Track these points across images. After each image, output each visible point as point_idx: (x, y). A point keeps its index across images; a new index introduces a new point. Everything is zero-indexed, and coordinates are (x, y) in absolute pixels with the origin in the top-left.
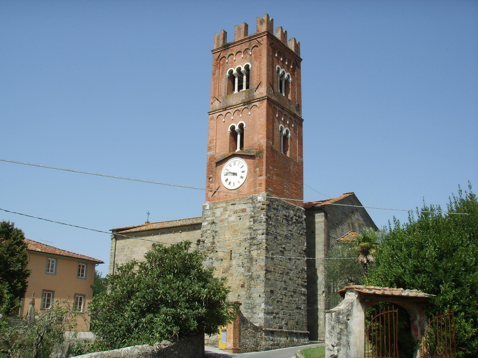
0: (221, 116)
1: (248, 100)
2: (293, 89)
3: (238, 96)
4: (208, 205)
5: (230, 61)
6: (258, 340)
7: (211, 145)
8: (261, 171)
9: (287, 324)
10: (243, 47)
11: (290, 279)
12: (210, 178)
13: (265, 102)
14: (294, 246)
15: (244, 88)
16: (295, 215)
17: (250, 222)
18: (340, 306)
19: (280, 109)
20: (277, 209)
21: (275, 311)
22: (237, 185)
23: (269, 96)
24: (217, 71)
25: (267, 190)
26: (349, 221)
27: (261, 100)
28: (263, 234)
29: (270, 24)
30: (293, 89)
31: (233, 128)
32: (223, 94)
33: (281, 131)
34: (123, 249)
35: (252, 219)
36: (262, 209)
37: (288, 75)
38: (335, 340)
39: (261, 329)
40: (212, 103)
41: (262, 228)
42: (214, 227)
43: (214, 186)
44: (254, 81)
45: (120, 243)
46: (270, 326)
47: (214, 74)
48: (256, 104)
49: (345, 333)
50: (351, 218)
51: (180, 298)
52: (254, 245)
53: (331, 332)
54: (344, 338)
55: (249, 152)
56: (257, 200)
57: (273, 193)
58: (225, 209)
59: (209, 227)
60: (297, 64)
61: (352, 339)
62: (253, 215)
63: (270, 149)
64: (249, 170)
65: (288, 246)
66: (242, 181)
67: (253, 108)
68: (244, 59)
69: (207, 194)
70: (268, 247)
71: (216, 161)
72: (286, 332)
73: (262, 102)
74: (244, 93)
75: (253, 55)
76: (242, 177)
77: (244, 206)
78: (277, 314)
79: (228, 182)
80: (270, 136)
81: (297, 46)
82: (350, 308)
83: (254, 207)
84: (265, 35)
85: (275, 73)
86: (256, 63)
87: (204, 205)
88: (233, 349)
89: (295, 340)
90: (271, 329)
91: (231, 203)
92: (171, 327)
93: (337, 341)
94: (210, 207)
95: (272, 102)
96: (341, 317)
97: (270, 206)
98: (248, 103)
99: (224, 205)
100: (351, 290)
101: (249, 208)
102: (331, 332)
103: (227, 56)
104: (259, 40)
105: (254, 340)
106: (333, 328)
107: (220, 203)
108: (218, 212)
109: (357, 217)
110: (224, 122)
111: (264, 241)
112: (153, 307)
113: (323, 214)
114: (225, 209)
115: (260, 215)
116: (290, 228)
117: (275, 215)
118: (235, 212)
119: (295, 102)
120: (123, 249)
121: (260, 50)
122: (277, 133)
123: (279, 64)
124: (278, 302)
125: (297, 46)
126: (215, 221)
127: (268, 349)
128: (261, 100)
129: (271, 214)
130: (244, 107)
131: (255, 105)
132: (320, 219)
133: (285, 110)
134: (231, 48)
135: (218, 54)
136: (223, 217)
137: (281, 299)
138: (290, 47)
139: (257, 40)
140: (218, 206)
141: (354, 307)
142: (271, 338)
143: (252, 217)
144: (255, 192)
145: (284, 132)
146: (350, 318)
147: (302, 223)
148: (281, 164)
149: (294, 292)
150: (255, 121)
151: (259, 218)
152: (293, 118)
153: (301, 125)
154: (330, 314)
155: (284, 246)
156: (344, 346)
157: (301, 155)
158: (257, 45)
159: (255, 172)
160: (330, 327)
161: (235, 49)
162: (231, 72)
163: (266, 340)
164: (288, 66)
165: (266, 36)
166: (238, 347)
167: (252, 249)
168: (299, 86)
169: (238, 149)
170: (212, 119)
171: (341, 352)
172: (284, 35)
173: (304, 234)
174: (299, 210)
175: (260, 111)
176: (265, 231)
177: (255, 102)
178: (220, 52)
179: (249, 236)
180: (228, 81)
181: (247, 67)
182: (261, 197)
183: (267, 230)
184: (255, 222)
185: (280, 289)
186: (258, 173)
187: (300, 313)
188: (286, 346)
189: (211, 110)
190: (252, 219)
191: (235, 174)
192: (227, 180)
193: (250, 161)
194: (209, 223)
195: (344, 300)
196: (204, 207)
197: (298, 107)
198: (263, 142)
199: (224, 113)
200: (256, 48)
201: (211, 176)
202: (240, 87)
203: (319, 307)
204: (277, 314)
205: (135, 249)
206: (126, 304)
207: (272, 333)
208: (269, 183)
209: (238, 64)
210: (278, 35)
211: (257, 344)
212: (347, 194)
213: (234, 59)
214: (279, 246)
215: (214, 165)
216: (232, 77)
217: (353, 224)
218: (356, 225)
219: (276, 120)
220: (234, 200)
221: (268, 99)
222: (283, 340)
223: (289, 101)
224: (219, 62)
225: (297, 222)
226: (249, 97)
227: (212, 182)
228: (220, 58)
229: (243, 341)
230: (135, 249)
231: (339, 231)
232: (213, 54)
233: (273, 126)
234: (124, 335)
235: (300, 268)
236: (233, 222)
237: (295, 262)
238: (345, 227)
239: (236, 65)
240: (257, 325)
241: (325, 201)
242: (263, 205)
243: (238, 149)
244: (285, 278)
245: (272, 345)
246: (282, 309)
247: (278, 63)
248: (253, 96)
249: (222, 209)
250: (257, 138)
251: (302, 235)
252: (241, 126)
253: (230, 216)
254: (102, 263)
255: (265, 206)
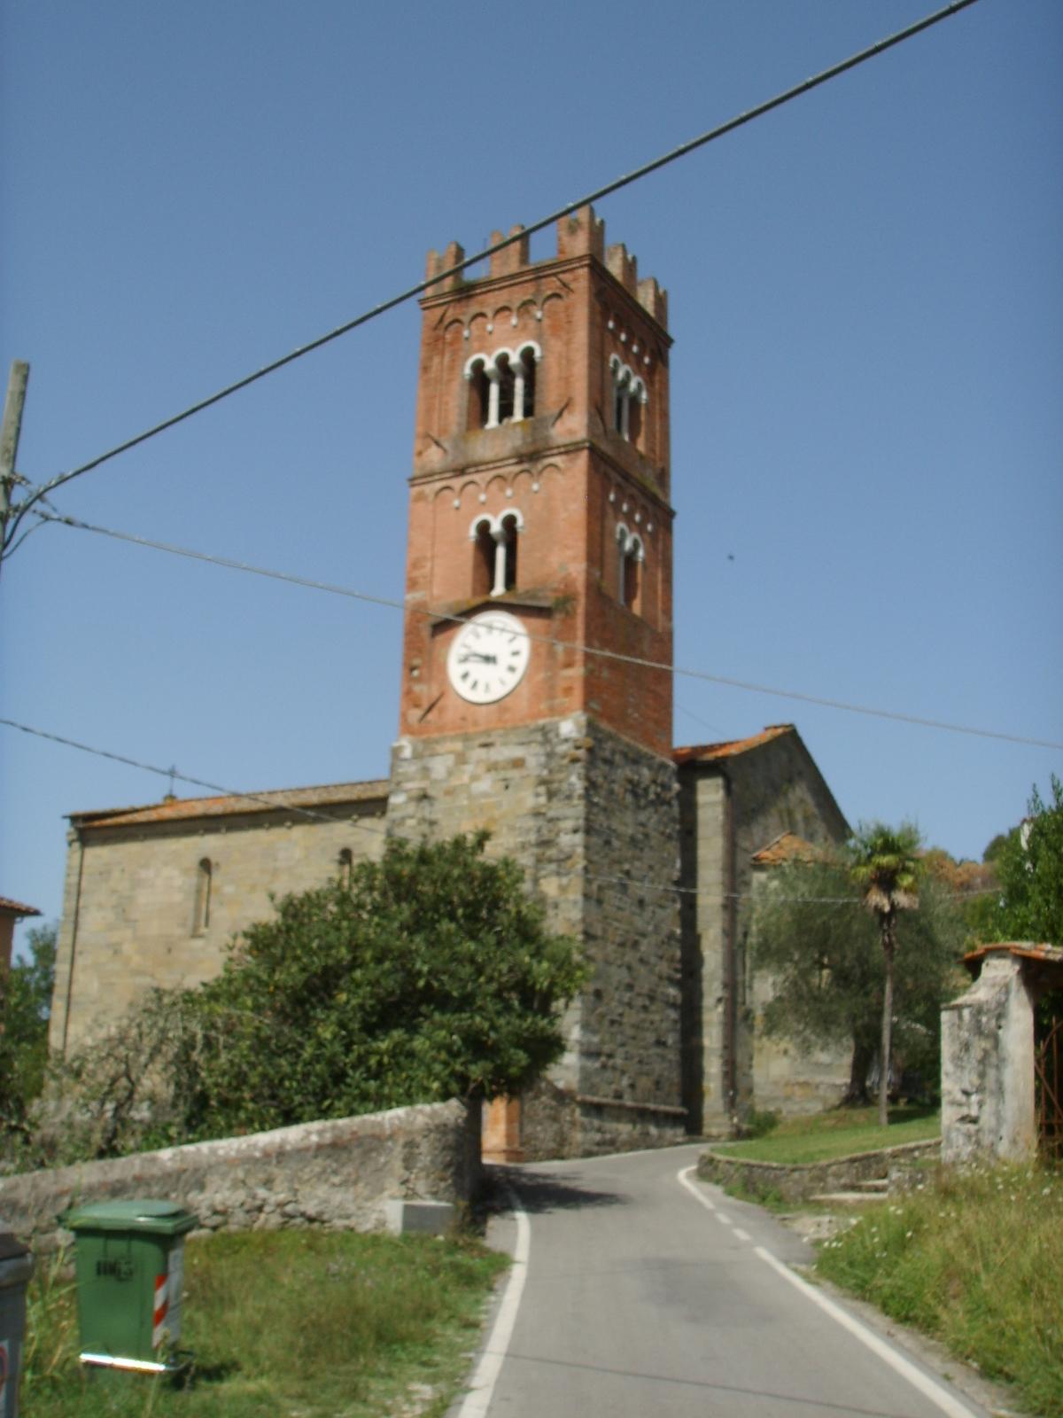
0: (446, 492)
1: (531, 449)
2: (650, 424)
3: (499, 436)
4: (407, 746)
5: (476, 333)
6: (566, 1129)
7: (416, 573)
8: (570, 652)
9: (632, 1086)
10: (517, 296)
11: (642, 961)
12: (412, 669)
13: (583, 457)
14: (651, 868)
15: (518, 415)
16: (654, 782)
17: (537, 795)
18: (975, 992)
19: (619, 479)
20: (609, 762)
21: (606, 1048)
22: (497, 692)
23: (595, 441)
24: (436, 360)
25: (586, 707)
26: (782, 805)
27: (570, 450)
28: (575, 831)
29: (597, 234)
30: (650, 424)
31: (484, 527)
32: (454, 429)
33: (621, 542)
34: (105, 874)
35: (542, 789)
36: (575, 760)
37: (639, 384)
38: (970, 1079)
39: (573, 1099)
40: (420, 454)
41: (573, 813)
42: (426, 811)
43: (425, 691)
44: (549, 396)
45: (99, 855)
46: (593, 1089)
47: (426, 369)
48: (557, 460)
49: (993, 1060)
50: (785, 794)
51: (480, 986)
52: (550, 861)
53: (959, 1058)
54: (992, 1073)
55: (533, 597)
56: (557, 735)
57: (601, 715)
58: (461, 759)
59: (411, 809)
60: (659, 350)
61: (1009, 1077)
62: (548, 778)
63: (595, 591)
64: (535, 652)
65: (637, 868)
66: (512, 680)
67: (545, 473)
68: (520, 330)
69: (404, 716)
70: (591, 867)
71: (433, 621)
72: (631, 1109)
73: (572, 456)
74: (518, 429)
75: (546, 322)
76: (512, 669)
77: (518, 752)
78: (610, 1056)
79: (470, 681)
80: (596, 552)
81: (661, 301)
82: (1003, 998)
83: (550, 755)
84: (582, 267)
85: (608, 376)
86: (557, 345)
87: (396, 744)
88: (504, 1151)
89: (653, 1130)
90: (596, 1099)
91: (478, 742)
92: (463, 1064)
93: (976, 1081)
94: (414, 750)
95: (602, 459)
96: (984, 1019)
97: (596, 753)
98: (532, 457)
99: (458, 746)
100: (1001, 953)
101: (534, 757)
102: (959, 1058)
103: (465, 319)
104: (566, 277)
105: (556, 1126)
106: (966, 1047)
107: (444, 739)
108: (440, 766)
109: (799, 792)
110: (457, 508)
111: (580, 850)
112: (397, 1011)
113: (719, 781)
114: (461, 759)
115: (568, 777)
116: (642, 817)
117: (605, 777)
118: (492, 767)
119: (654, 461)
120: (105, 874)
121: (567, 308)
122: (610, 546)
123: (616, 350)
124: (613, 1022)
125: (661, 301)
126: (431, 792)
127: (588, 1154)
128: (570, 450)
129: (594, 774)
130: (517, 468)
131: (551, 465)
132: (710, 794)
133: (630, 483)
134: (480, 298)
135: (438, 312)
136: (455, 782)
137: (621, 1015)
138: (641, 301)
139: (560, 280)
140: (439, 748)
141: (1012, 996)
142: (596, 1123)
143: (543, 782)
144: (553, 711)
145: (628, 545)
146: (1003, 1023)
147: (669, 803)
148: (618, 633)
149: (652, 998)
150: (553, 514)
151: (565, 786)
152: (650, 507)
153: (668, 528)
154: (955, 1013)
155: (626, 866)
156: (992, 1093)
157: (668, 612)
158: (558, 291)
159: (551, 654)
160: (956, 1047)
161: (492, 301)
162: (478, 366)
163: (584, 1129)
164: (639, 357)
165: (586, 270)
166: (516, 1146)
167: (543, 873)
168: (665, 415)
169: (499, 590)
170: (420, 497)
171: (986, 1108)
172: (630, 267)
173: (675, 835)
174: (663, 766)
175: (568, 484)
176: (581, 822)
177: (553, 455)
178: (444, 308)
179: (533, 837)
180: (470, 390)
181: (528, 355)
182: (570, 727)
183: (587, 819)
184: (551, 795)
185: (617, 989)
186: (561, 657)
187: (663, 1057)
188: (633, 1145)
189: (417, 473)
190: (542, 789)
191: (489, 659)
192: (465, 676)
193: (538, 623)
194: (410, 799)
195: (980, 980)
196: (396, 752)
197: (663, 477)
198: (577, 570)
199: (457, 483)
200: (554, 301)
201: (416, 662)
202: (506, 411)
203: (707, 1042)
204: (610, 1056)
205: (143, 874)
206: (321, 1001)
207: (596, 1109)
208: (592, 689)
209: (501, 341)
210: (615, 267)
211: (562, 1140)
212: (776, 727)
213: (489, 327)
214: (616, 867)
215: (426, 632)
216: (480, 380)
217: (790, 813)
218: (799, 816)
219: (610, 511)
220: (487, 733)
221: (593, 450)
222: (625, 1129)
223: (641, 457)
224: (442, 336)
225: (660, 801)
226: (534, 441)
227: (419, 680)
228: (446, 322)
229: (528, 1129)
230: (143, 874)
231: (757, 830)
232: (425, 309)
233: (603, 527)
234: (324, 1087)
235: (665, 930)
236: (486, 795)
237: (654, 912)
238: (772, 820)
239: (493, 347)
240: (561, 1085)
241: (302, 790)
242: (578, 748)
243: (499, 590)
244: (631, 957)
245: (598, 1144)
246: (623, 1045)
247: (615, 346)
248: (547, 439)
249: (450, 760)
250: (558, 557)
251: (669, 837)
252: (510, 522)
253: (475, 778)
254: (1034, 785)
255: (581, 753)
